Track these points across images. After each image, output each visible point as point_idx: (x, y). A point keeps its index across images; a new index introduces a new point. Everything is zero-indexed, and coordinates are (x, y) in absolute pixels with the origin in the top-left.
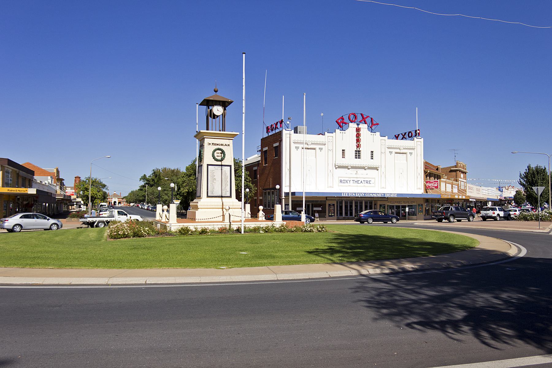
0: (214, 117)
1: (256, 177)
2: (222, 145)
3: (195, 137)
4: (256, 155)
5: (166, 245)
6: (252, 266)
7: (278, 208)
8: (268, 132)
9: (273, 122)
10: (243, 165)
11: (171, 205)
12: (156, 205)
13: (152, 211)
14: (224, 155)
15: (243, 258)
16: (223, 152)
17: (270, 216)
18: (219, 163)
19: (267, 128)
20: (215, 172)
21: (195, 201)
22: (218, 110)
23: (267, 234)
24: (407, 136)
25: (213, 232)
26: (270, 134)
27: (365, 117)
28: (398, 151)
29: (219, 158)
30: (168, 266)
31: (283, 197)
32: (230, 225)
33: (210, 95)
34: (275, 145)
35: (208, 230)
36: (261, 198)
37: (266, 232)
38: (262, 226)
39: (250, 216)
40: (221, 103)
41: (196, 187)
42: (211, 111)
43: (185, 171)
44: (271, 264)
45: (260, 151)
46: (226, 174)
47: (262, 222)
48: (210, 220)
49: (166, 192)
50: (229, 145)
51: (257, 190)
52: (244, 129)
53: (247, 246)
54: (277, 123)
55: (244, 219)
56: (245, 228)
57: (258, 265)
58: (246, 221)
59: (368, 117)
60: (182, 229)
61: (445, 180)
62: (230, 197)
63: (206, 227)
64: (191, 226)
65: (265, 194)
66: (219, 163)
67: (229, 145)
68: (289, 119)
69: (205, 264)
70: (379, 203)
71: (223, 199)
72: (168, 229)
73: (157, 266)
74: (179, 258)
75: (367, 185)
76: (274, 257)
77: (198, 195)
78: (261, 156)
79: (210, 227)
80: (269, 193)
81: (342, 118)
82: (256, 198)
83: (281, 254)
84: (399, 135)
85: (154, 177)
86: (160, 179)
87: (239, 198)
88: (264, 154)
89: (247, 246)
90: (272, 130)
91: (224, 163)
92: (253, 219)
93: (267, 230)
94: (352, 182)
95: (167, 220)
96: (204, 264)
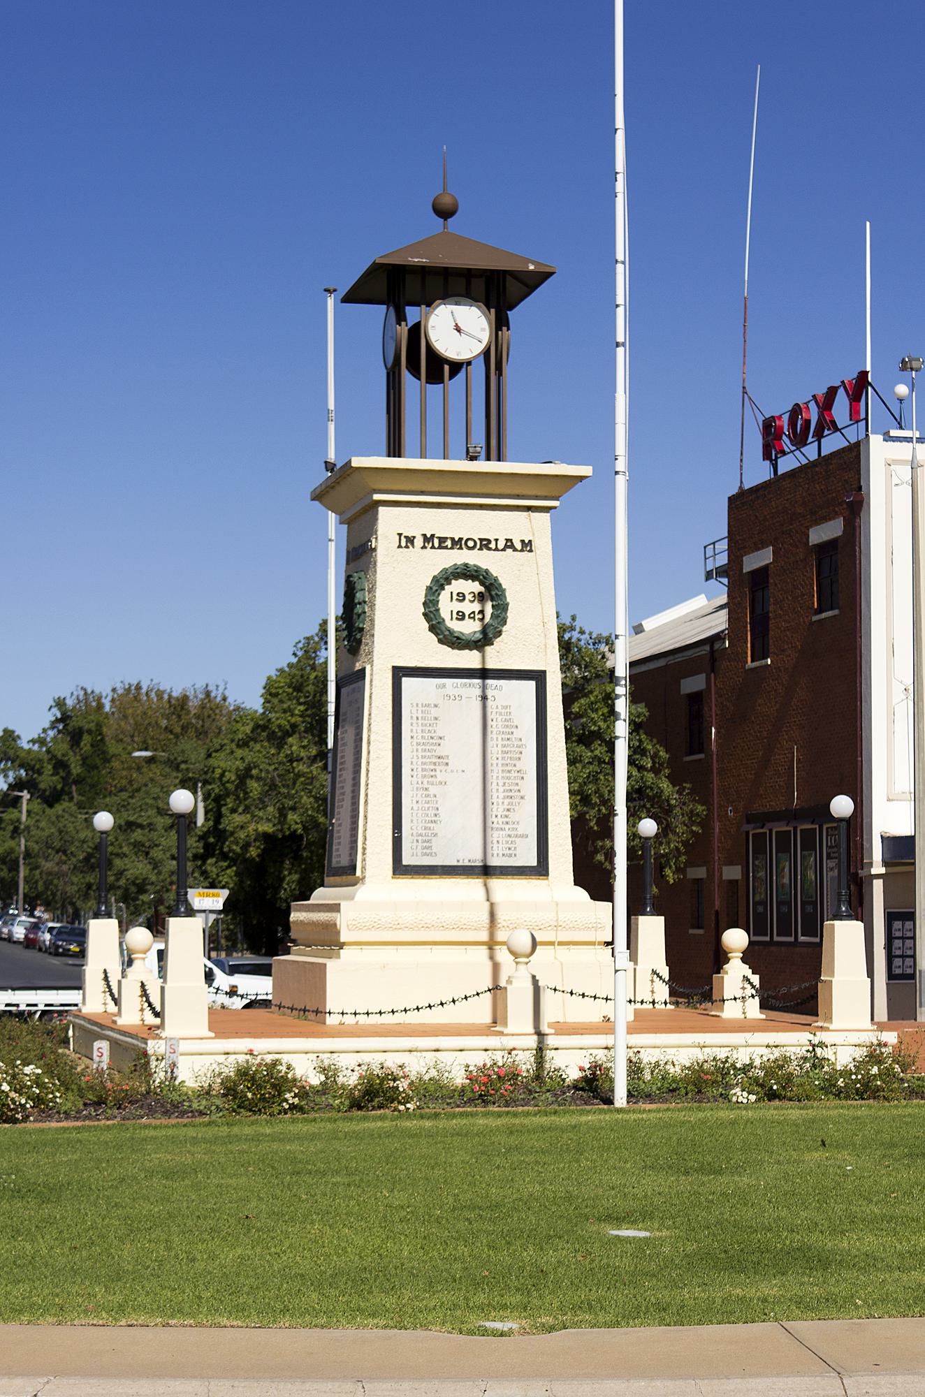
0: (438, 368)
1: (697, 742)
2: (485, 544)
3: (319, 496)
4: (699, 603)
5: (150, 1174)
6: (681, 1316)
7: (846, 941)
8: (771, 450)
9: (805, 390)
10: (620, 664)
11: (174, 923)
12: (76, 916)
13: (54, 951)
14: (501, 609)
15: (625, 1264)
16: (491, 590)
17: (794, 988)
18: (469, 659)
19: (770, 429)
20: (445, 711)
21: (320, 895)
22: (457, 329)
23: (773, 1110)
25: (432, 1092)
26: (787, 464)
29: (470, 628)
30: (161, 1310)
31: (878, 869)
32: (540, 1050)
33: (408, 237)
34: (820, 534)
35: (403, 1085)
36: (733, 873)
37: (772, 1096)
38: (742, 1058)
39: (663, 992)
40: (479, 285)
41: (325, 804)
42: (416, 332)
43: (254, 702)
44: (807, 1307)
45: (721, 572)
46: (511, 726)
47: (741, 1030)
48: (426, 1017)
49: (137, 835)
50: (527, 546)
51: (706, 823)
52: (621, 447)
53: (652, 1184)
54: (832, 392)
55: (625, 1015)
56: (635, 1069)
57: (728, 1312)
58: (644, 1022)
60: (243, 1073)
62: (541, 869)
63: (392, 1061)
64: (301, 1058)
65: (760, 849)
66: (469, 659)
67: (527, 546)
68: (905, 366)
69: (390, 1301)
71: (497, 884)
72: (159, 1076)
73: (98, 1309)
74: (229, 1256)
76: (821, 1262)
77: (339, 857)
78: (732, 606)
79: (413, 1061)
80: (784, 839)
82: (700, 873)
83: (870, 1242)
85: (63, 748)
86: (99, 756)
87: (593, 878)
88: (749, 592)
89: (652, 1184)
90: (800, 440)
91: (496, 657)
92: (686, 1013)
93: (774, 1085)
95: (151, 1019)
96: (378, 1298)
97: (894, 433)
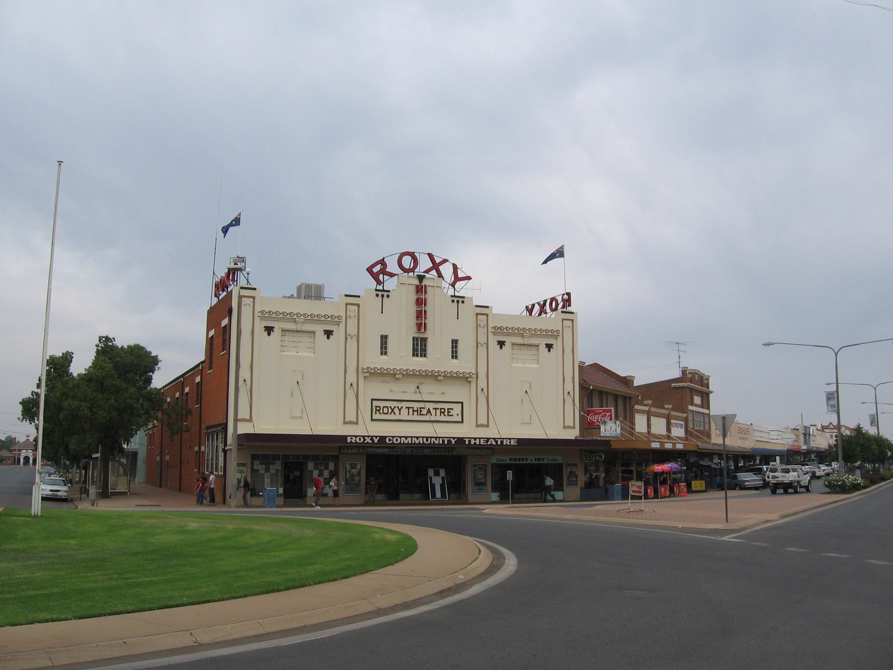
24: (537, 308)
27: (438, 260)
28: (519, 340)
59: (445, 261)
61: (647, 408)
81: (382, 262)
84: (533, 306)
94: (404, 411)
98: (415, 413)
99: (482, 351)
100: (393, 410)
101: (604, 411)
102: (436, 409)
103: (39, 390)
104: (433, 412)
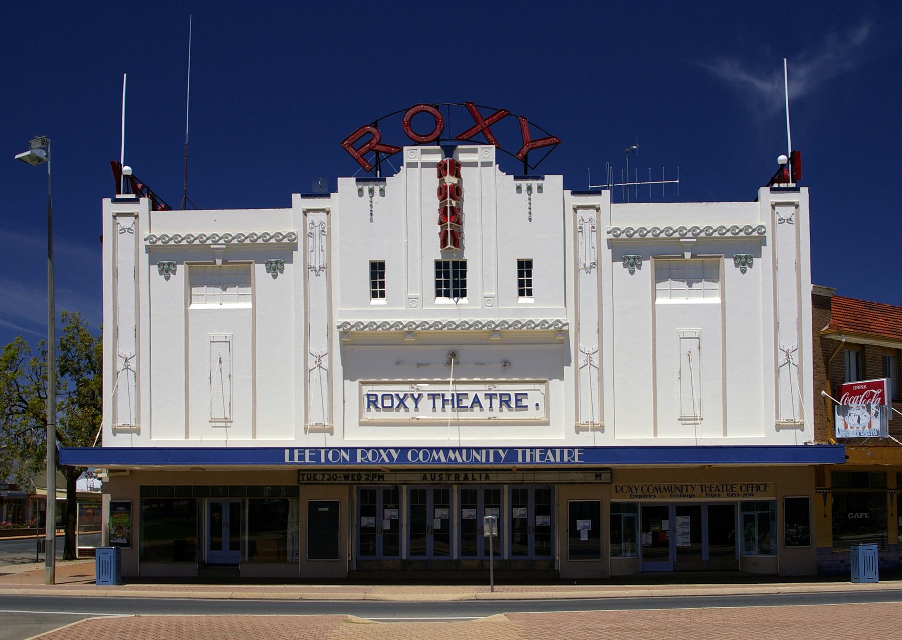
70: (308, 494)
75: (506, 414)
94: (426, 403)
97: (118, 196)
98: (449, 407)
99: (588, 281)
100: (402, 401)
101: (870, 386)
102: (490, 396)
103: (467, 513)
104: (485, 403)
